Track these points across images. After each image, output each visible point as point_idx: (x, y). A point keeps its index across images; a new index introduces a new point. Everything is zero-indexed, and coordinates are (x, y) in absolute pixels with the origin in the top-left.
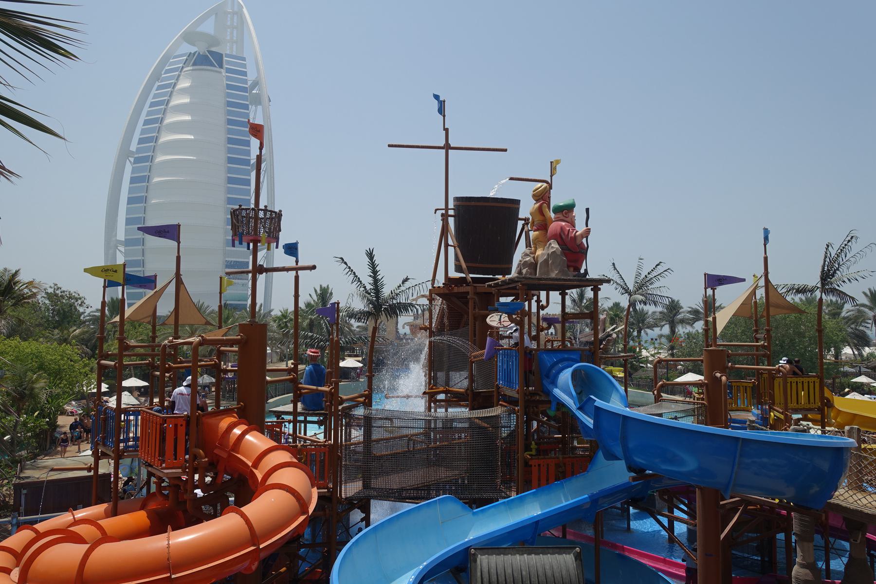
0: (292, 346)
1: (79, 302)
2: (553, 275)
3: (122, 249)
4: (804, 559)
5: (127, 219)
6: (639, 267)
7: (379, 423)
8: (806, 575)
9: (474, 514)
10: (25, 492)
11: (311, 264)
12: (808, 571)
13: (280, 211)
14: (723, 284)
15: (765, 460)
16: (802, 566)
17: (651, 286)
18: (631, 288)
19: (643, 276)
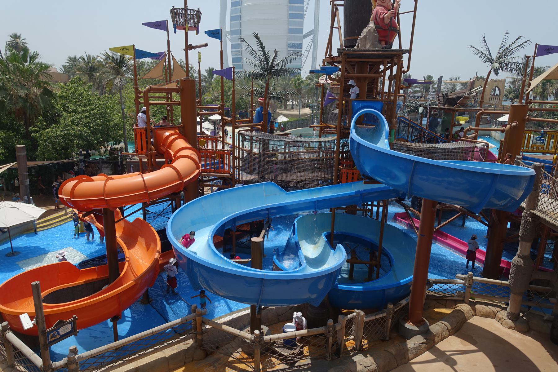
0: (320, 99)
1: (193, 70)
2: (367, 48)
3: (229, 37)
4: (520, 252)
5: (231, 17)
6: (505, 40)
7: (341, 148)
8: (519, 262)
9: (286, 194)
10: (132, 165)
11: (204, 43)
12: (521, 260)
13: (199, 9)
14: (550, 53)
15: (451, 179)
16: (519, 257)
17: (511, 56)
18: (494, 57)
19: (507, 46)
